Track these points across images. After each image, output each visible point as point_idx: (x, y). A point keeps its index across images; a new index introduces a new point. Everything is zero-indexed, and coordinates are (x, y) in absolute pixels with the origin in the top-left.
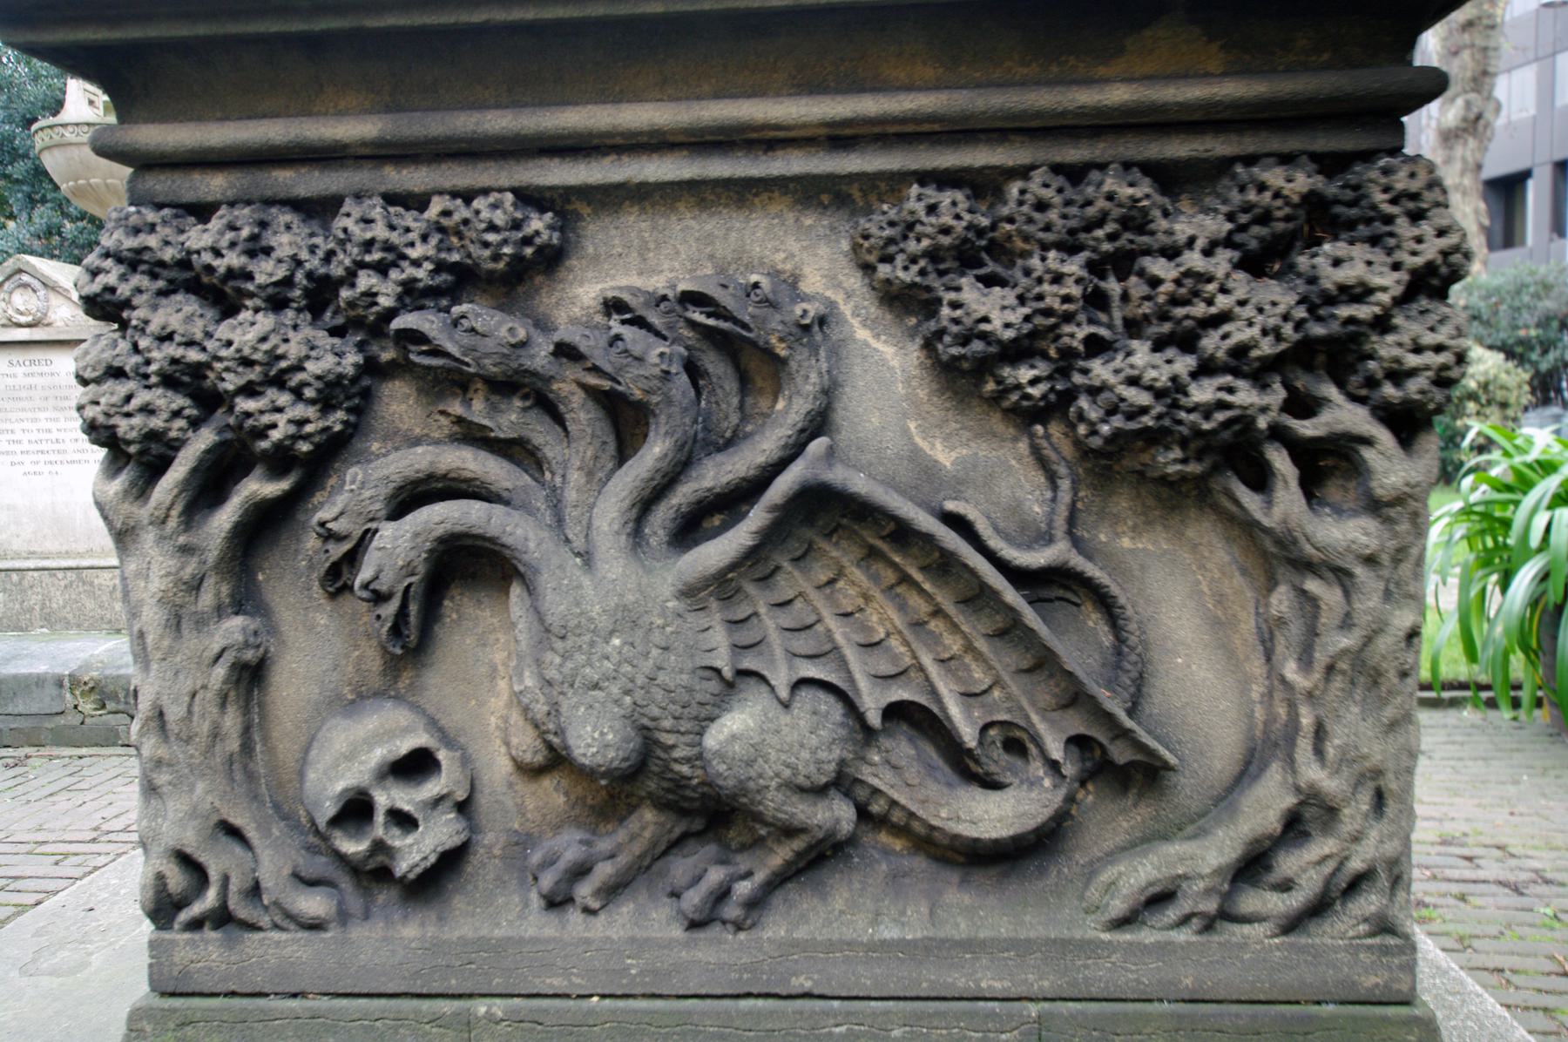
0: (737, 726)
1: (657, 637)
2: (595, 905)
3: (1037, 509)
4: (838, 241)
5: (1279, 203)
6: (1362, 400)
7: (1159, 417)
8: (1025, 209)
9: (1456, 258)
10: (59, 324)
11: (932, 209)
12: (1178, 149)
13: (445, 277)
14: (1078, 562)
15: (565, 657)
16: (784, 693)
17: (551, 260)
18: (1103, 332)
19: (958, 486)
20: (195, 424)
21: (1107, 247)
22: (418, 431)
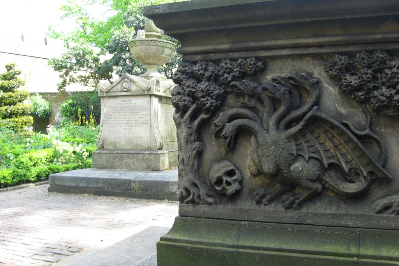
1: (281, 147)
2: (267, 203)
3: (363, 123)
4: (321, 66)
7: (388, 102)
8: (360, 59)
10: (133, 91)
11: (340, 60)
13: (241, 74)
14: (371, 134)
15: (262, 150)
16: (307, 159)
17: (262, 71)
18: (377, 85)
19: (346, 117)
20: (192, 103)
21: (377, 67)
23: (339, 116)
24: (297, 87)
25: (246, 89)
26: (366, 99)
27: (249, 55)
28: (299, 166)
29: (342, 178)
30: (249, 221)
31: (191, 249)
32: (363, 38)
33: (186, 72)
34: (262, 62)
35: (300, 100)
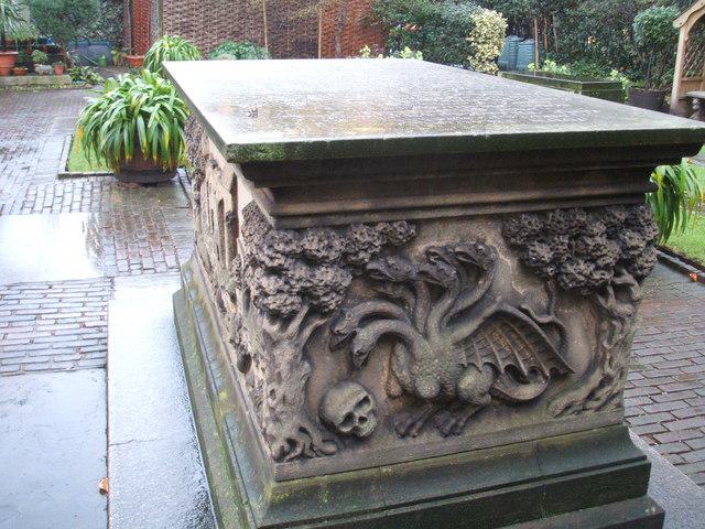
11: (530, 223)
12: (593, 204)
14: (556, 320)
17: (412, 240)
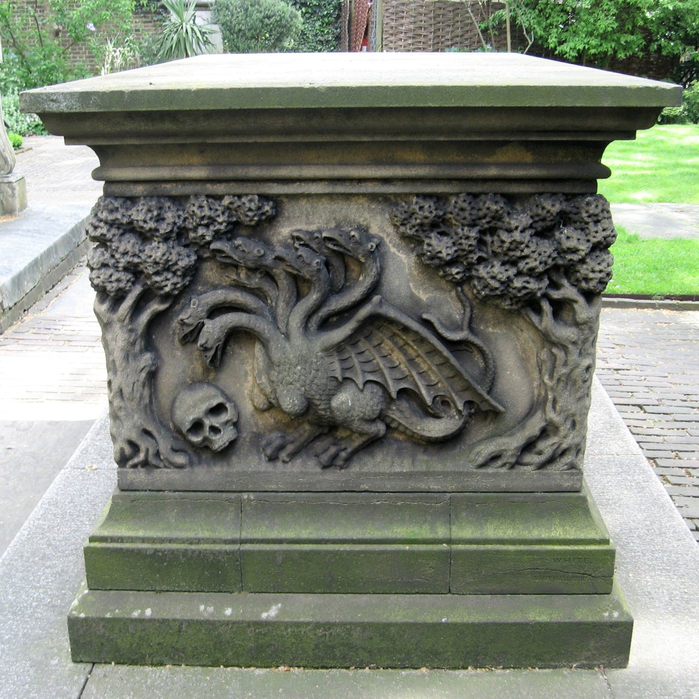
0: (344, 399)
1: (314, 366)
2: (288, 460)
3: (457, 317)
4: (384, 214)
5: (549, 215)
6: (575, 286)
7: (502, 291)
8: (457, 210)
9: (609, 239)
11: (421, 208)
12: (515, 189)
13: (230, 227)
14: (472, 338)
15: (279, 373)
16: (361, 387)
17: (272, 220)
18: (484, 255)
19: (428, 307)
20: (134, 283)
21: (486, 226)
22: (217, 282)
23: (415, 308)
24: (341, 256)
25: (244, 258)
26: (464, 278)
27: (247, 191)
28: (348, 400)
29: (420, 411)
30: (256, 492)
31: (154, 553)
32: (465, 173)
33: (117, 222)
34: (271, 203)
35: (345, 277)
